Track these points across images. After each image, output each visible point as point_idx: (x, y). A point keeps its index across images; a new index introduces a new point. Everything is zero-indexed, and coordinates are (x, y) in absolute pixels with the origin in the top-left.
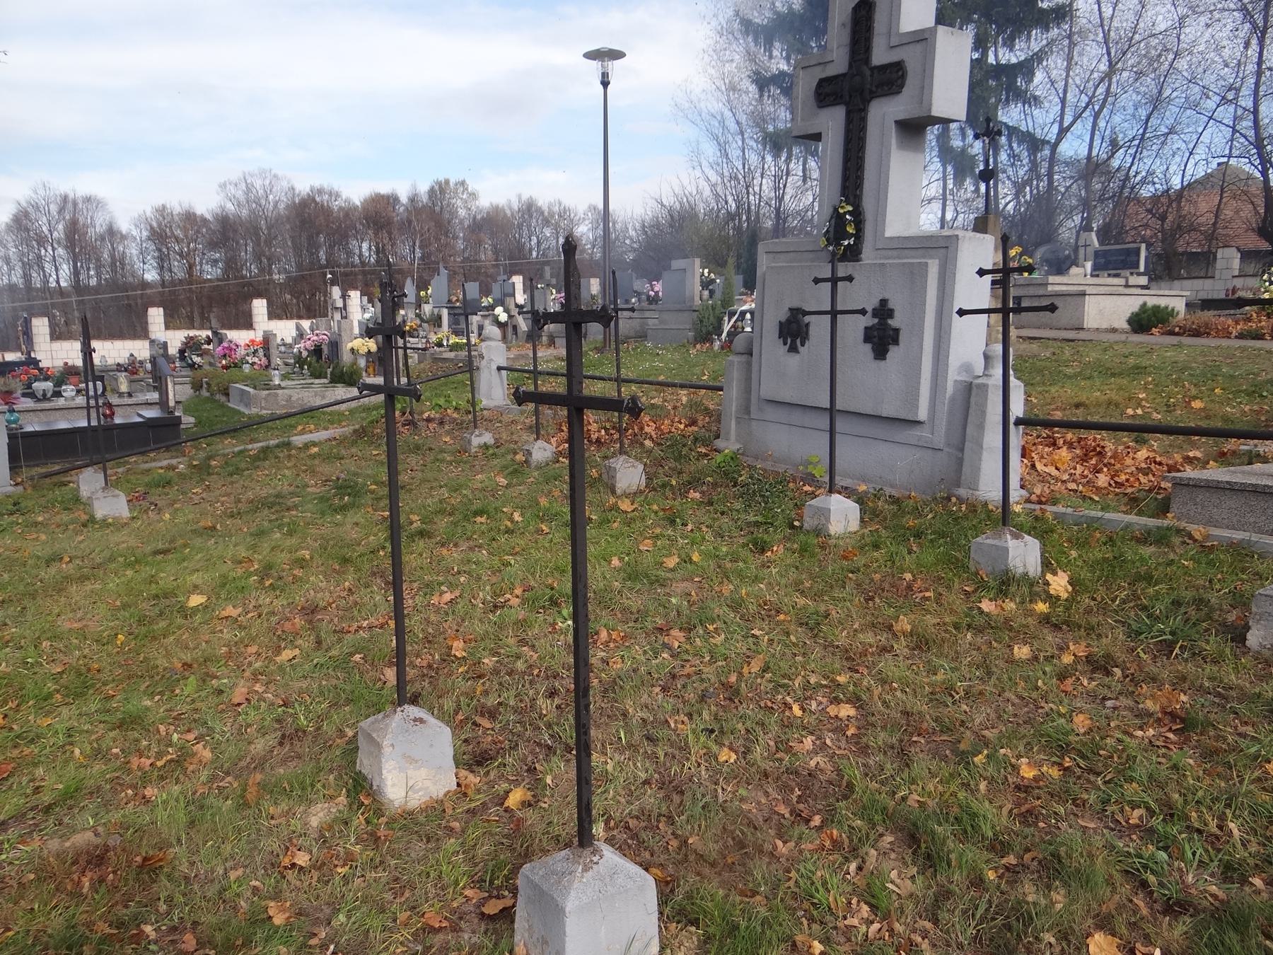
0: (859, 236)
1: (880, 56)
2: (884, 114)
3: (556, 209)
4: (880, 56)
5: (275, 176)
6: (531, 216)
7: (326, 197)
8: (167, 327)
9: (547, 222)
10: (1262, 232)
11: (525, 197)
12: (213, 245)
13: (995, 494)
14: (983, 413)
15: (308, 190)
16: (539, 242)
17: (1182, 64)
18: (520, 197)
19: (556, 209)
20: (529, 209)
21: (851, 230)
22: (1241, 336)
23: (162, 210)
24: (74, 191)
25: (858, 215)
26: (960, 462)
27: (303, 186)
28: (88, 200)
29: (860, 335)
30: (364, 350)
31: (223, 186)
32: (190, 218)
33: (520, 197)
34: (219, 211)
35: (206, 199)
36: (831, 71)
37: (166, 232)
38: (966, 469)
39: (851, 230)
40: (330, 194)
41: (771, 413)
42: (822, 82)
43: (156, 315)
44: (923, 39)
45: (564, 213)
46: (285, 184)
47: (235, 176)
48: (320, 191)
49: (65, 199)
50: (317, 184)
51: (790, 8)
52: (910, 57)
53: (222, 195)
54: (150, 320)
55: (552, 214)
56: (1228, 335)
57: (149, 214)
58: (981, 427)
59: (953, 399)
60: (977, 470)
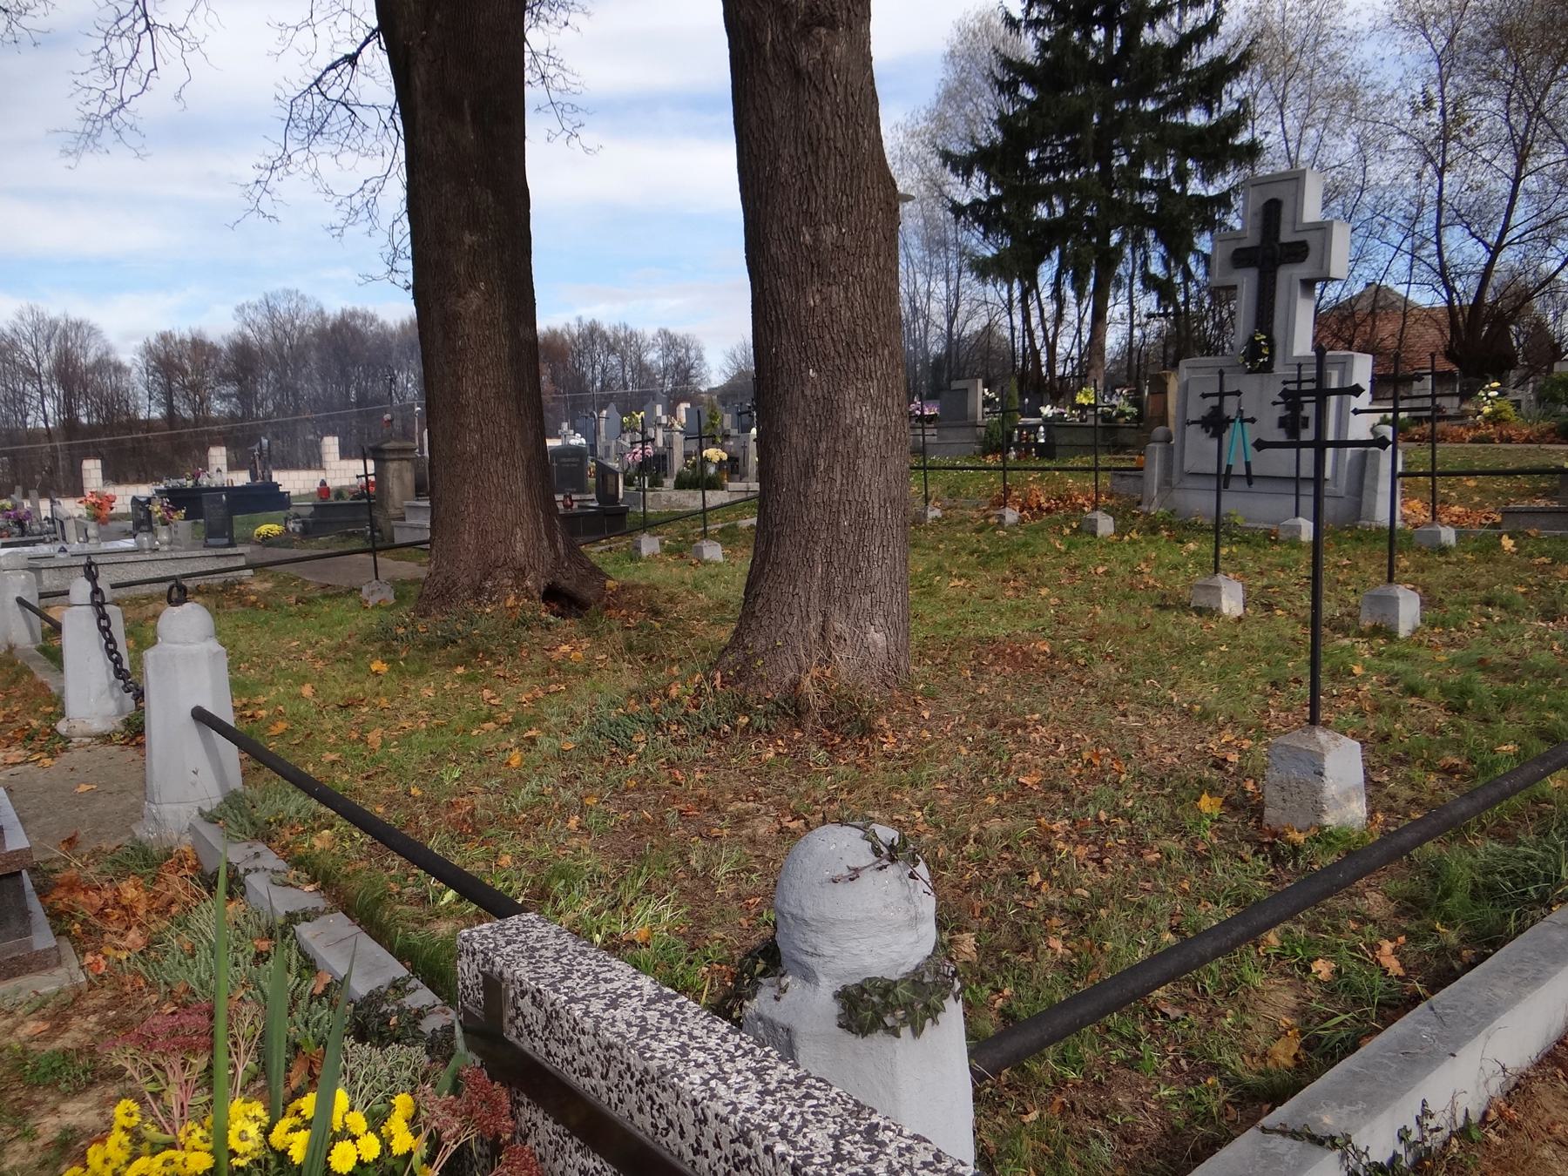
0: (1271, 355)
1: (1286, 236)
2: (1289, 276)
3: (622, 334)
4: (1286, 236)
5: (303, 298)
6: (594, 343)
7: (359, 322)
8: (342, 458)
9: (612, 350)
10: (1449, 355)
11: (587, 320)
12: (224, 378)
13: (1387, 523)
14: (1377, 471)
15: (339, 313)
16: (604, 370)
17: (1367, 198)
18: (580, 319)
19: (622, 334)
20: (593, 334)
21: (1265, 351)
22: (1474, 441)
23: (165, 338)
24: (66, 315)
25: (1271, 343)
26: (1359, 505)
27: (335, 306)
28: (79, 326)
29: (1275, 422)
30: (716, 459)
31: (240, 310)
32: (199, 346)
33: (580, 319)
34: (239, 340)
35: (220, 322)
36: (1245, 244)
37: (175, 363)
38: (1364, 508)
39: (1265, 351)
40: (365, 318)
41: (1190, 482)
42: (1237, 252)
43: (92, 470)
44: (1323, 229)
45: (631, 338)
46: (313, 307)
47: (255, 298)
48: (354, 315)
49: (54, 325)
50: (349, 307)
51: (992, 142)
52: (1312, 239)
53: (240, 319)
54: (85, 474)
55: (617, 340)
56: (1463, 441)
57: (152, 341)
58: (1376, 478)
59: (1351, 462)
60: (1373, 508)
